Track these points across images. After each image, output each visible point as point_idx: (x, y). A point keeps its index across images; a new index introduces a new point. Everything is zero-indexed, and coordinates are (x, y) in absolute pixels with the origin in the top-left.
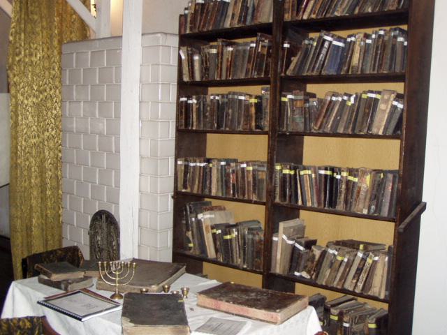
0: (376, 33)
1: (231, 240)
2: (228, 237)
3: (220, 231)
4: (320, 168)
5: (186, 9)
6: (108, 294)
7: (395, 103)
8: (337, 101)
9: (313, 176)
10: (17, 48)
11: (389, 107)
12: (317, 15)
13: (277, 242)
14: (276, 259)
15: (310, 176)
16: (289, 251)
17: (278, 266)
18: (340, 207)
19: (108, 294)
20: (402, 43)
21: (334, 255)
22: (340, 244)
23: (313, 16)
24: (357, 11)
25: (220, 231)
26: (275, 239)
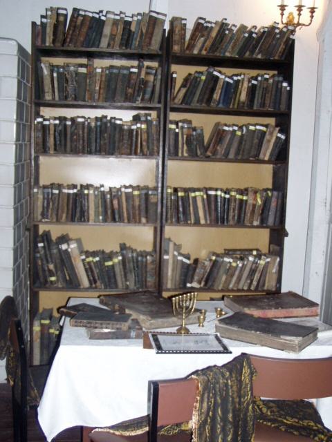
0: (262, 76)
1: (113, 266)
2: (110, 263)
3: (97, 259)
4: (211, 189)
5: (45, 17)
6: (174, 330)
7: (279, 135)
8: (229, 131)
9: (205, 197)
10: (75, 36)
11: (274, 138)
12: (208, 52)
13: (168, 260)
14: (167, 276)
15: (202, 197)
16: (179, 266)
17: (169, 282)
18: (225, 224)
19: (174, 330)
20: (286, 87)
21: (230, 263)
22: (228, 252)
23: (204, 52)
24: (247, 54)
25: (97, 259)
26: (166, 257)
